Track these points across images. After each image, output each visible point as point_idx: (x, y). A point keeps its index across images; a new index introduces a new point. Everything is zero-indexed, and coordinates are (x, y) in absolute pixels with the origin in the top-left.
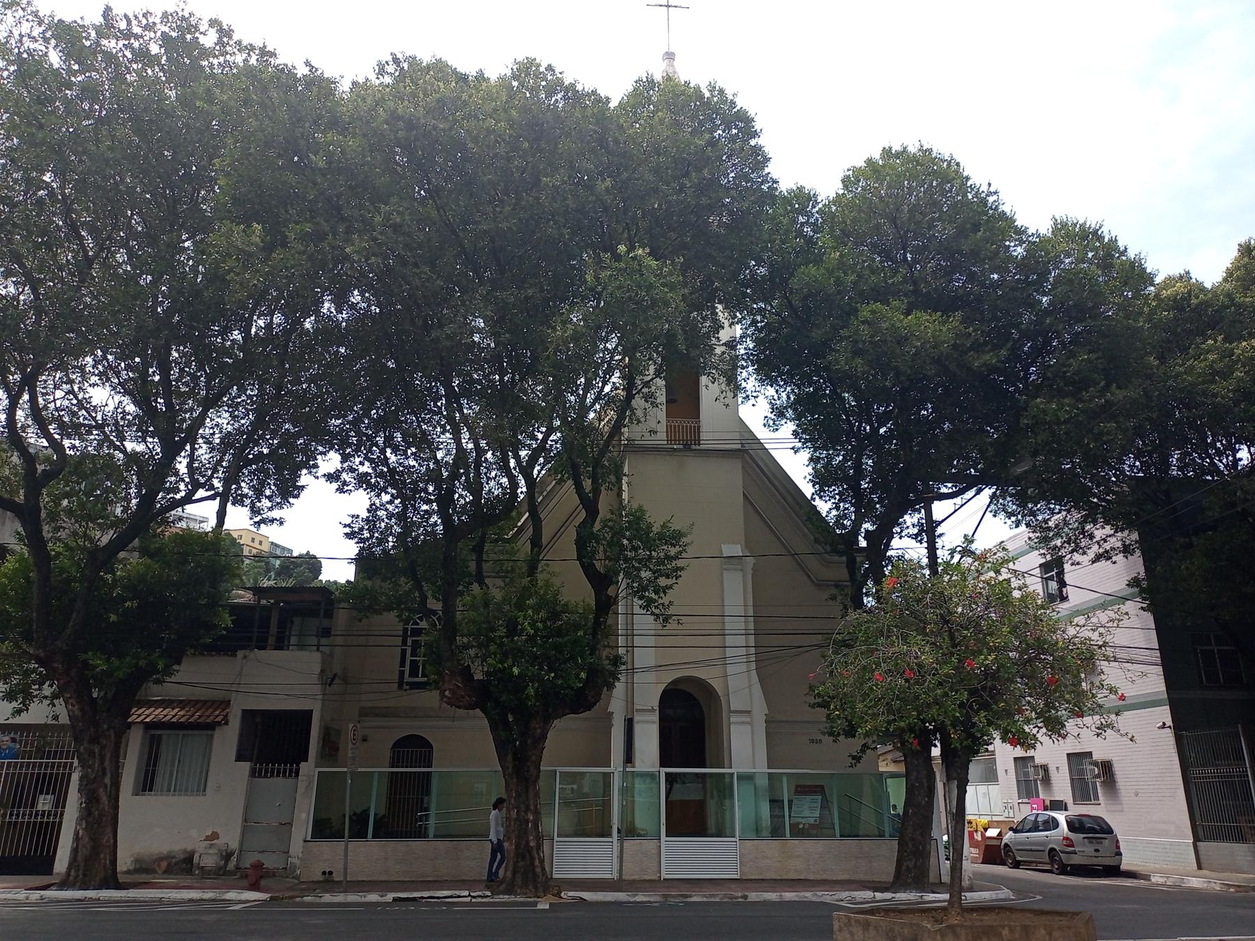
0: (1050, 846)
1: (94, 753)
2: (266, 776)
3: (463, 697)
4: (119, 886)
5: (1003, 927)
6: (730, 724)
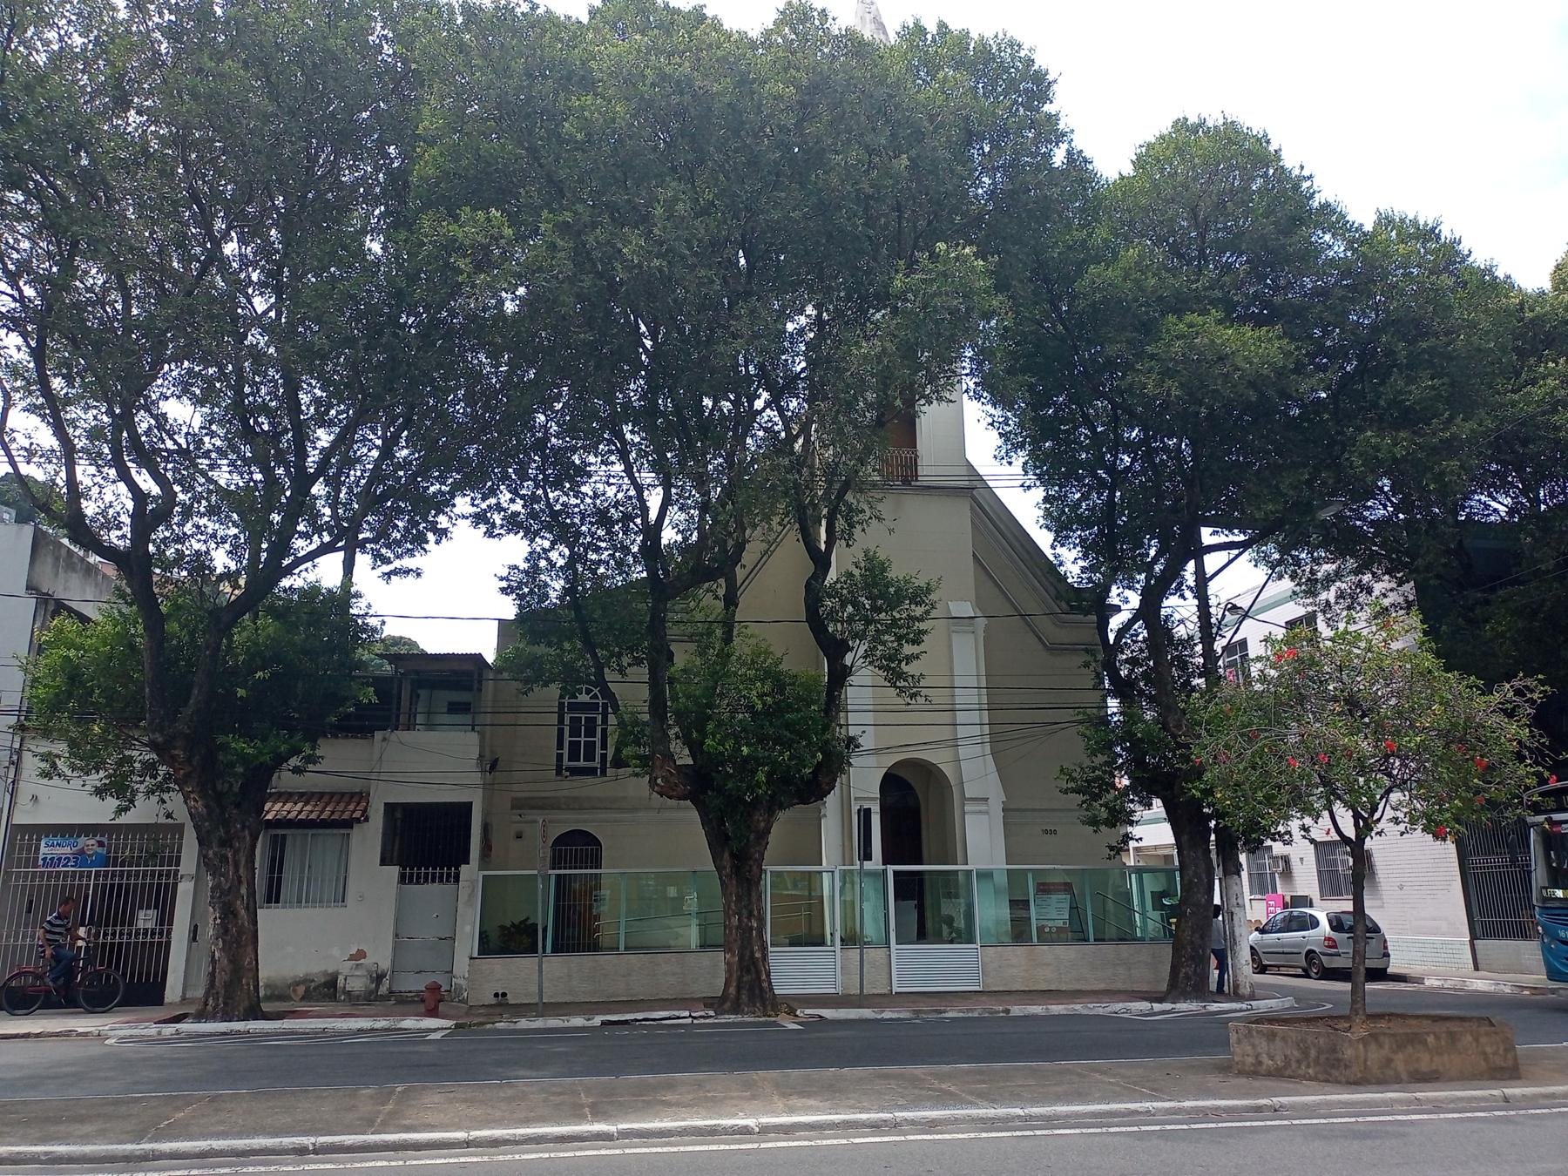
0: (1308, 948)
1: (228, 858)
2: (418, 883)
3: (676, 785)
5: (1428, 1034)
6: (964, 813)
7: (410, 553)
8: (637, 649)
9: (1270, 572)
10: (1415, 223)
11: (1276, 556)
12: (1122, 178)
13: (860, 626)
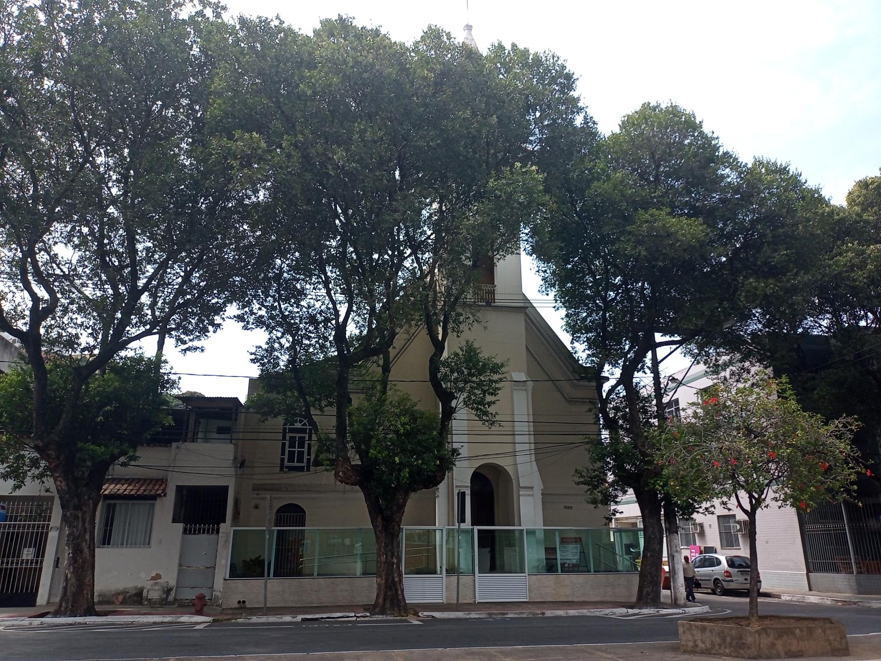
1: (78, 517)
2: (194, 533)
4: (97, 614)
5: (796, 628)
6: (519, 496)
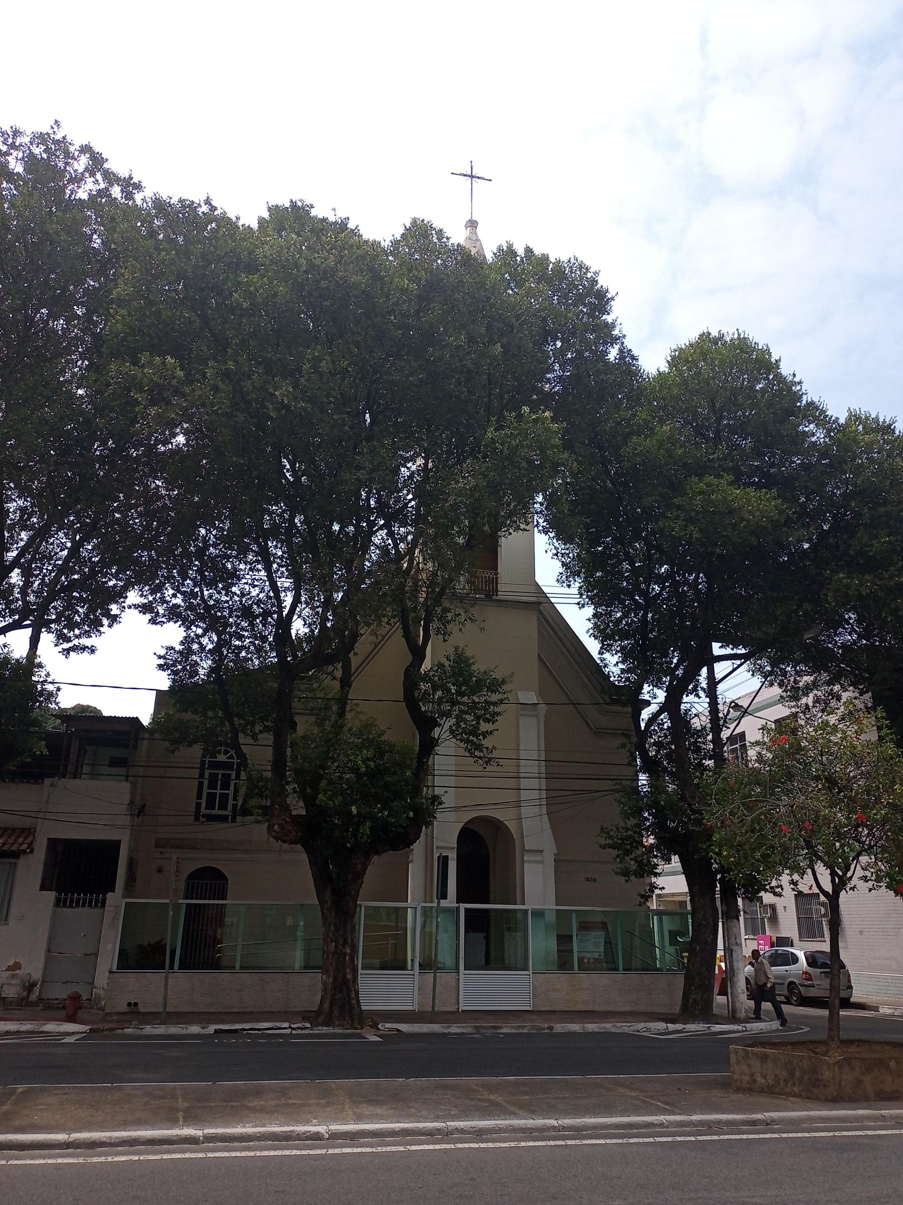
0: (790, 979)
2: (71, 906)
3: (290, 832)
6: (523, 862)
7: (88, 634)
8: (268, 719)
9: (763, 680)
10: (876, 420)
11: (769, 668)
12: (660, 374)
13: (446, 707)
